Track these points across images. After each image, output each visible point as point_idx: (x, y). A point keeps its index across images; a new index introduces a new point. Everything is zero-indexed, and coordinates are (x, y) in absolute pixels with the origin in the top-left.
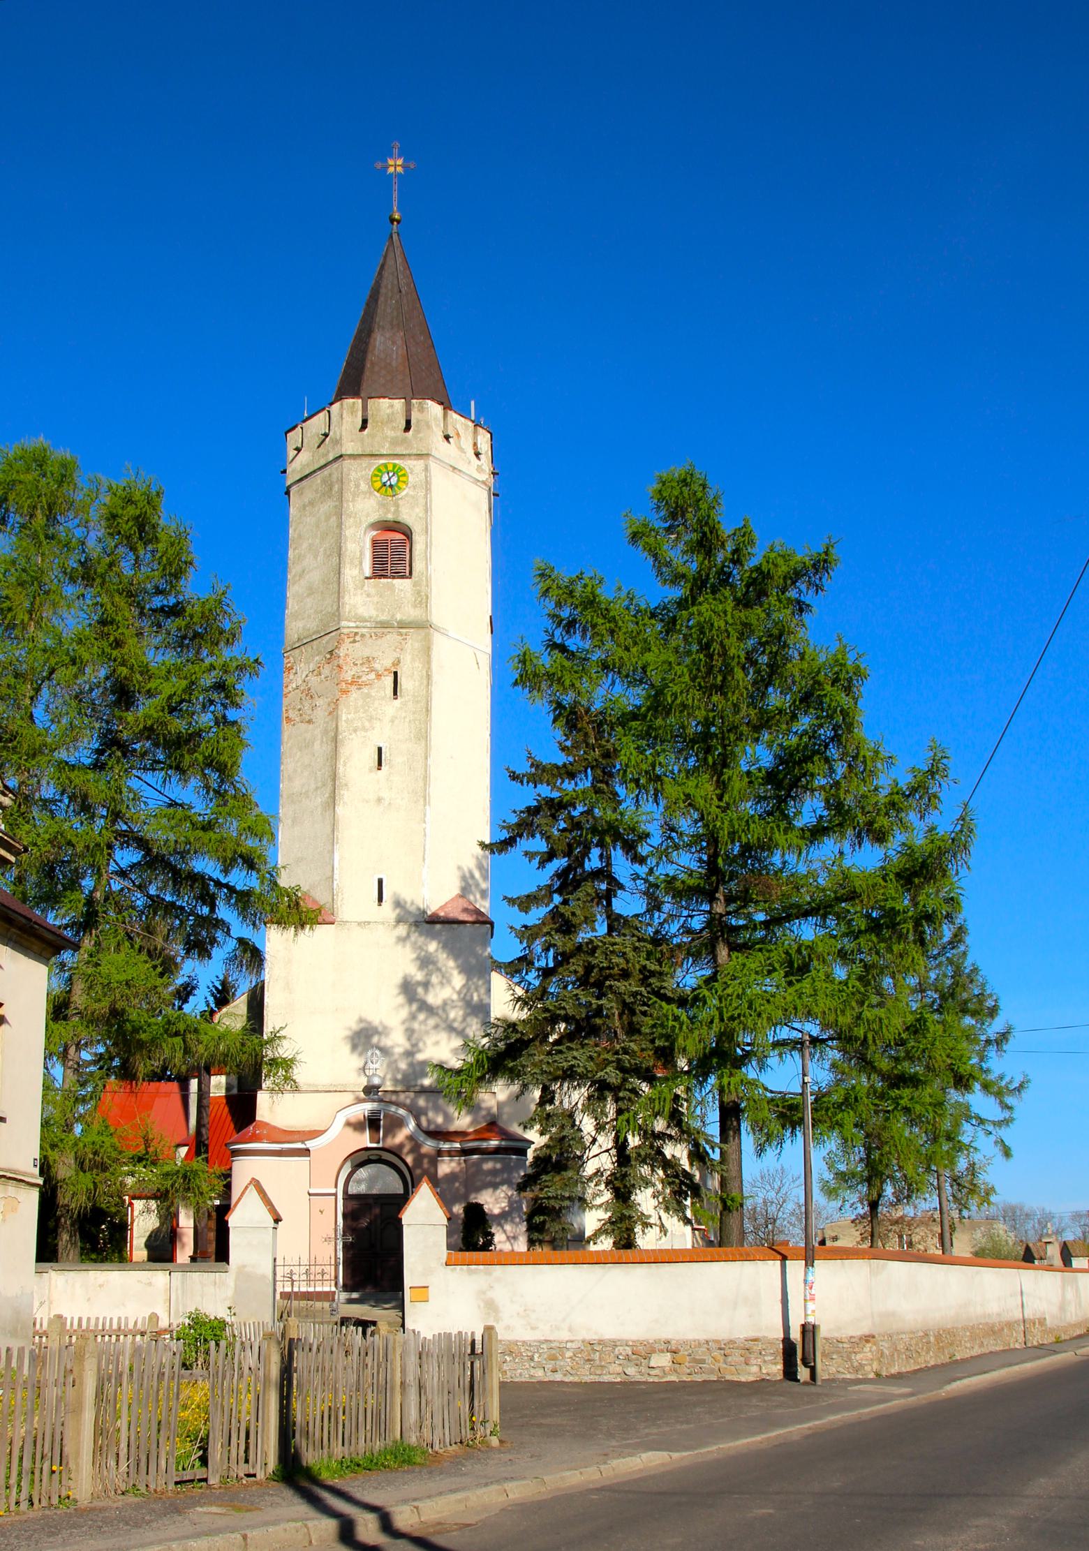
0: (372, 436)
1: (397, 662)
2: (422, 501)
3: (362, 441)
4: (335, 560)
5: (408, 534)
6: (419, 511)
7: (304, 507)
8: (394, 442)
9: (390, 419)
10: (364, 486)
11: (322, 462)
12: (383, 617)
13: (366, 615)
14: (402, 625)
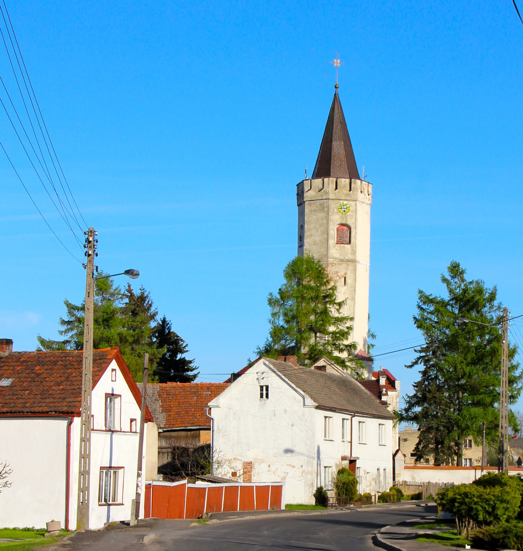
0: (339, 192)
1: (346, 274)
2: (354, 217)
3: (336, 194)
4: (326, 236)
5: (349, 228)
6: (353, 220)
7: (312, 211)
8: (346, 195)
9: (345, 186)
10: (336, 211)
11: (320, 198)
12: (341, 258)
13: (336, 257)
14: (348, 261)
